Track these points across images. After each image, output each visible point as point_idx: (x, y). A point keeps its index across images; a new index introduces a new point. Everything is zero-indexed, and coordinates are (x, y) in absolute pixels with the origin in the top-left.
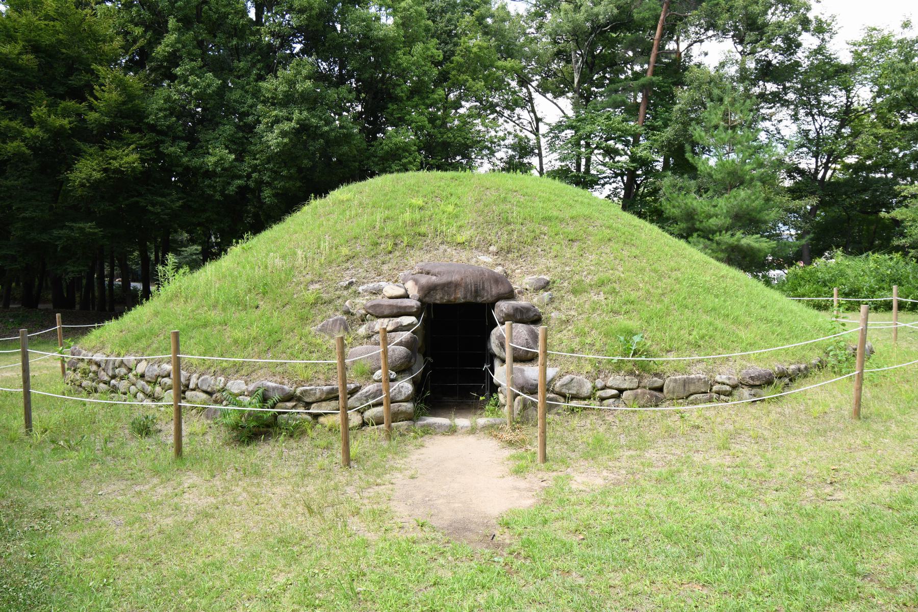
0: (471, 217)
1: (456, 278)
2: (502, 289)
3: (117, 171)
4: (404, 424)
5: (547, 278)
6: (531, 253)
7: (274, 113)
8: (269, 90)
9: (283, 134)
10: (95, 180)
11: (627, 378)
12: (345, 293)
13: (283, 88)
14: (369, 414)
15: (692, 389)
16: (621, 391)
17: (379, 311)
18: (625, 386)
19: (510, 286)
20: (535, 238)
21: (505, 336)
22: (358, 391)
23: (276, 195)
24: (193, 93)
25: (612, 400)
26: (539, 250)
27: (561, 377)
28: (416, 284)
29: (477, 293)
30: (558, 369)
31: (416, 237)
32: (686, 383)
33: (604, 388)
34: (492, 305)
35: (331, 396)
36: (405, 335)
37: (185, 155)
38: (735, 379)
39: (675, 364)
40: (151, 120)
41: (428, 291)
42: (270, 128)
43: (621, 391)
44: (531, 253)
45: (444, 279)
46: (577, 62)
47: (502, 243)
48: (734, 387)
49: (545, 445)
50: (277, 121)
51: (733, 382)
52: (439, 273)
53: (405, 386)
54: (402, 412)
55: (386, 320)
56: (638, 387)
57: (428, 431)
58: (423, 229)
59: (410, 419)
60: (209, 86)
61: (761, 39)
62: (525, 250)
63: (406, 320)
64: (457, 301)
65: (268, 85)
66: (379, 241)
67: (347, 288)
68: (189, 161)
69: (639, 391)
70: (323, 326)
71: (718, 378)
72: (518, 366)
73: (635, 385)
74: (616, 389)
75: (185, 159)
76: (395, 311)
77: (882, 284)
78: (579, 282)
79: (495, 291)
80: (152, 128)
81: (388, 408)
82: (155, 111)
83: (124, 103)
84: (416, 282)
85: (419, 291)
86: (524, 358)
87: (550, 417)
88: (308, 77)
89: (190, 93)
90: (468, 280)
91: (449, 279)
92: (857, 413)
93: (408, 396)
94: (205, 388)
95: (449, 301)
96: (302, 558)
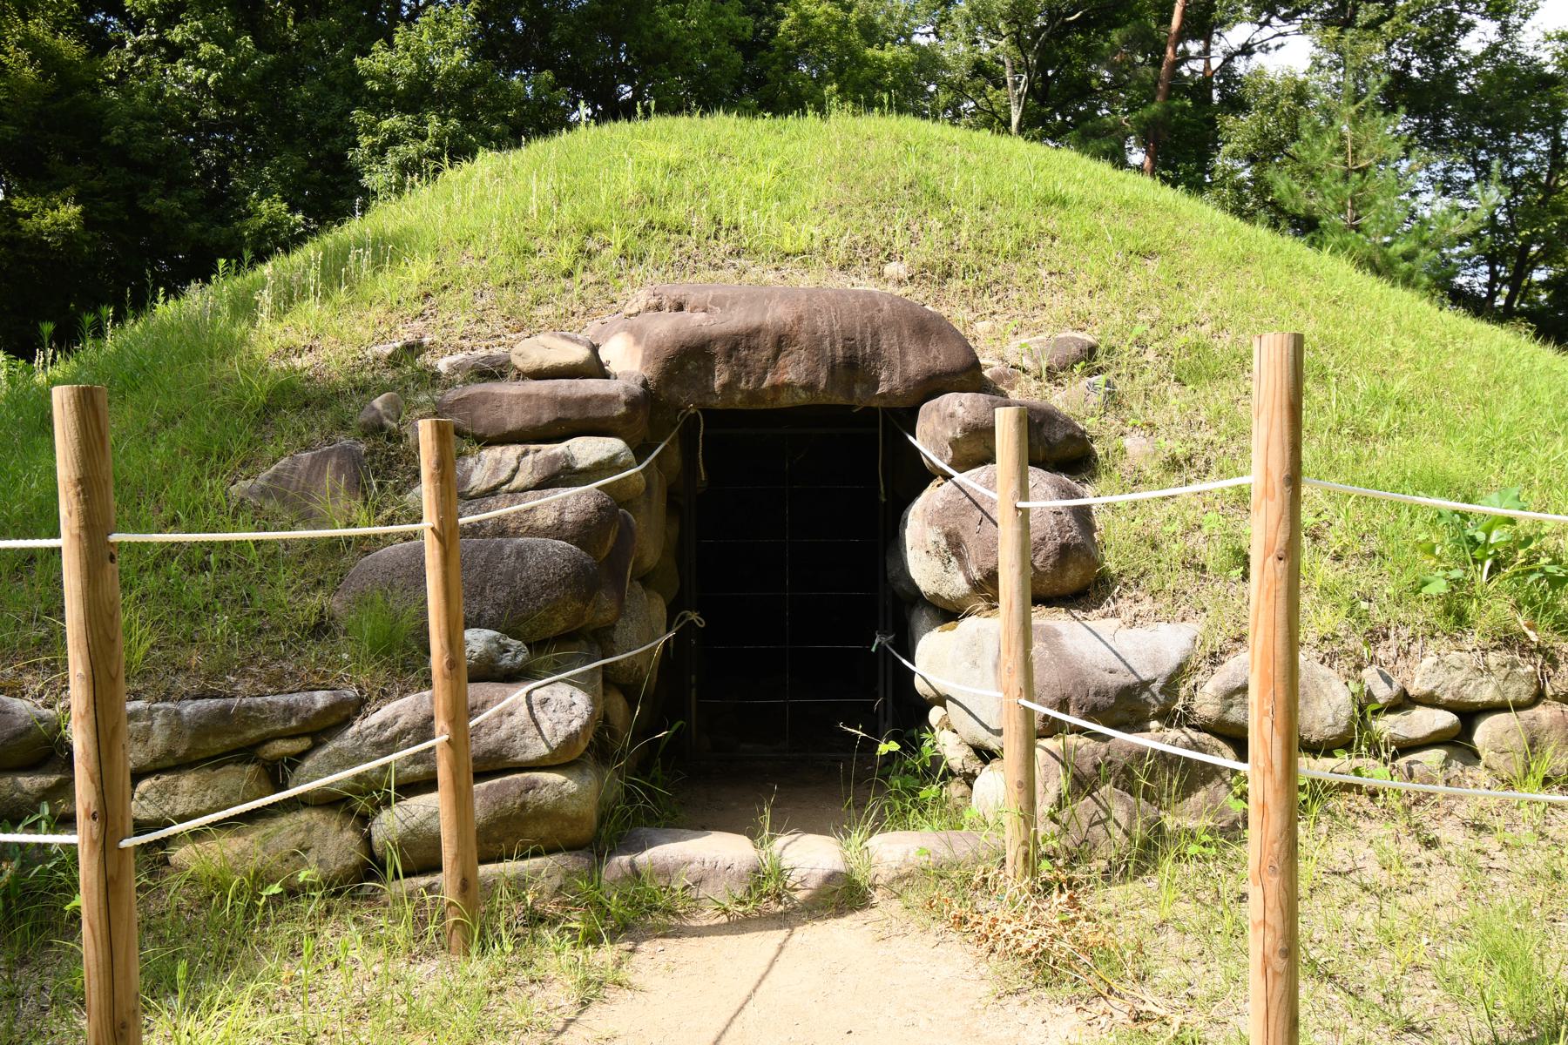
0: (819, 189)
2: (941, 358)
4: (543, 868)
5: (1089, 338)
6: (1018, 281)
7: (386, 124)
8: (374, 76)
11: (1493, 659)
13: (408, 66)
14: (391, 823)
16: (1469, 715)
18: (1486, 693)
19: (971, 352)
20: (1024, 244)
21: (963, 520)
22: (347, 722)
24: (210, 80)
25: (1434, 756)
26: (1044, 273)
27: (1215, 658)
28: (638, 342)
30: (1193, 628)
31: (655, 230)
33: (1403, 703)
34: (909, 418)
35: (216, 745)
36: (574, 500)
37: (194, 217)
40: (115, 136)
41: (686, 361)
42: (379, 152)
43: (1469, 715)
44: (1018, 281)
46: (1016, 85)
47: (925, 251)
49: (1293, 1023)
50: (394, 139)
52: (718, 302)
53: (558, 706)
54: (541, 814)
55: (513, 451)
56: (1538, 697)
57: (643, 916)
58: (676, 212)
59: (572, 847)
60: (244, 64)
61: (1392, 15)
62: (997, 272)
63: (587, 450)
64: (785, 400)
65: (378, 60)
66: (534, 246)
68: (204, 230)
69: (1545, 713)
70: (276, 478)
72: (1044, 618)
73: (1525, 691)
74: (1448, 707)
75: (194, 227)
76: (547, 416)
78: (1199, 348)
79: (916, 362)
80: (120, 155)
81: (462, 801)
82: (128, 120)
83: (55, 97)
84: (637, 335)
85: (646, 360)
86: (1073, 577)
87: (1320, 847)
89: (202, 84)
90: (822, 324)
91: (755, 320)
93: (571, 739)
95: (752, 395)
96: (1155, 377)
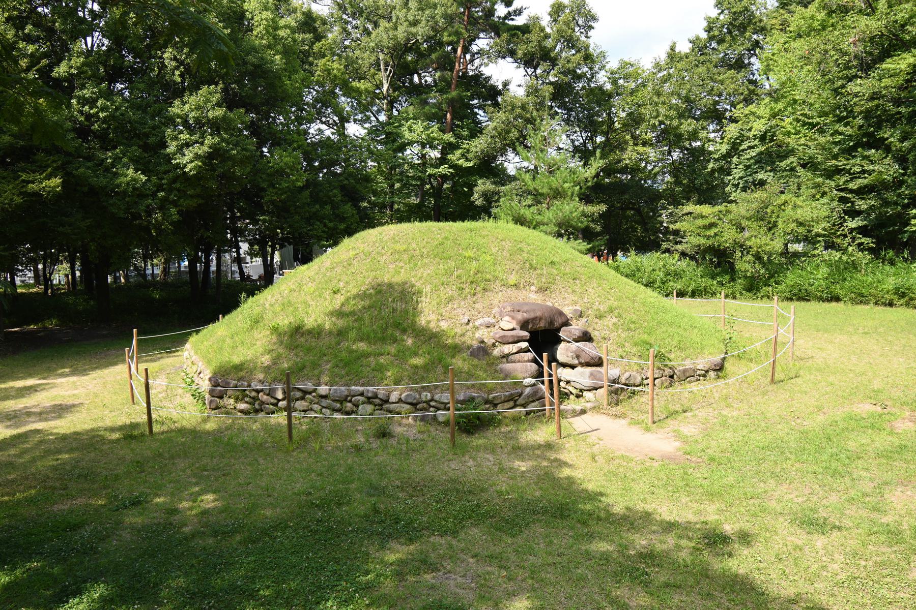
1: (539, 314)
3: (36, 194)
9: (197, 157)
10: (16, 205)
12: (468, 327)
15: (688, 375)
17: (505, 340)
23: (179, 213)
29: (551, 323)
32: (685, 371)
38: (707, 367)
39: (681, 363)
45: (532, 315)
48: (707, 372)
51: (706, 369)
55: (511, 345)
67: (468, 324)
71: (699, 367)
77: (668, 277)
88: (218, 104)
92: (772, 381)
94: (409, 401)
